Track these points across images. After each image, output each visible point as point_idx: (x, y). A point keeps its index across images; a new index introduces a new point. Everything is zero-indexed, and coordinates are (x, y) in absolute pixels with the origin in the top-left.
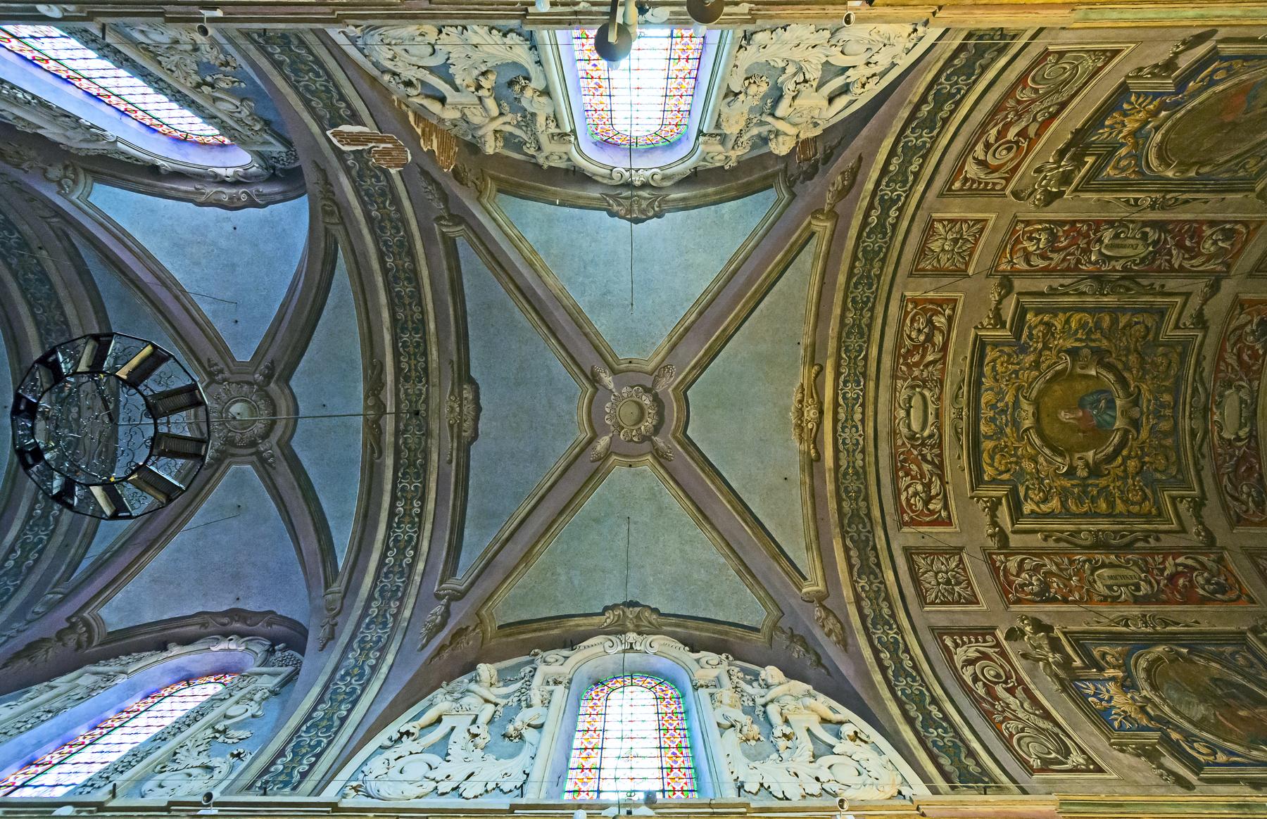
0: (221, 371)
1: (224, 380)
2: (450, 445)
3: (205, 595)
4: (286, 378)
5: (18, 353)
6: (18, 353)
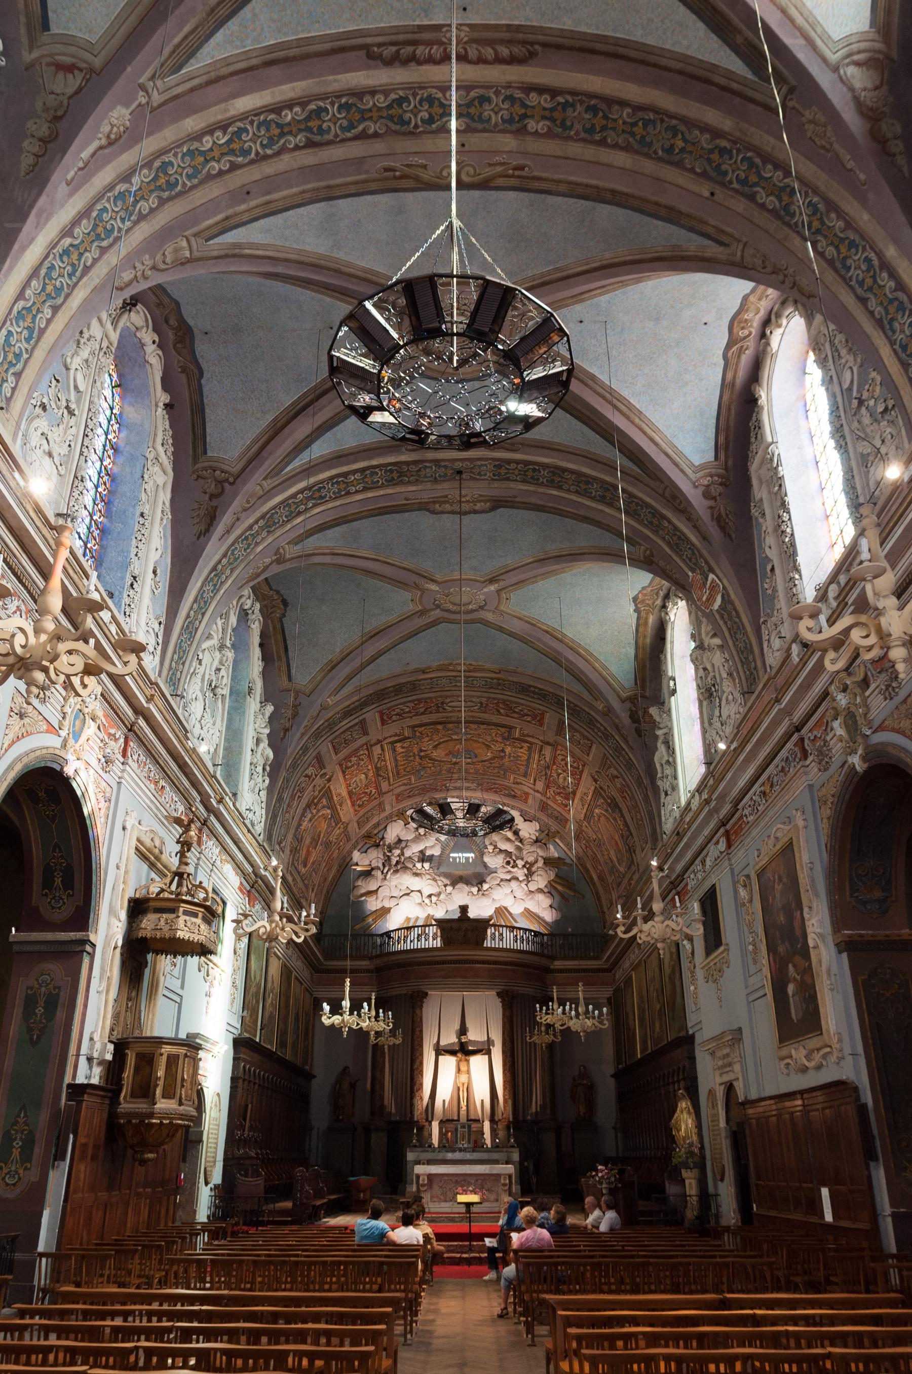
2: (426, 497)
5: (559, 47)
6: (559, 47)
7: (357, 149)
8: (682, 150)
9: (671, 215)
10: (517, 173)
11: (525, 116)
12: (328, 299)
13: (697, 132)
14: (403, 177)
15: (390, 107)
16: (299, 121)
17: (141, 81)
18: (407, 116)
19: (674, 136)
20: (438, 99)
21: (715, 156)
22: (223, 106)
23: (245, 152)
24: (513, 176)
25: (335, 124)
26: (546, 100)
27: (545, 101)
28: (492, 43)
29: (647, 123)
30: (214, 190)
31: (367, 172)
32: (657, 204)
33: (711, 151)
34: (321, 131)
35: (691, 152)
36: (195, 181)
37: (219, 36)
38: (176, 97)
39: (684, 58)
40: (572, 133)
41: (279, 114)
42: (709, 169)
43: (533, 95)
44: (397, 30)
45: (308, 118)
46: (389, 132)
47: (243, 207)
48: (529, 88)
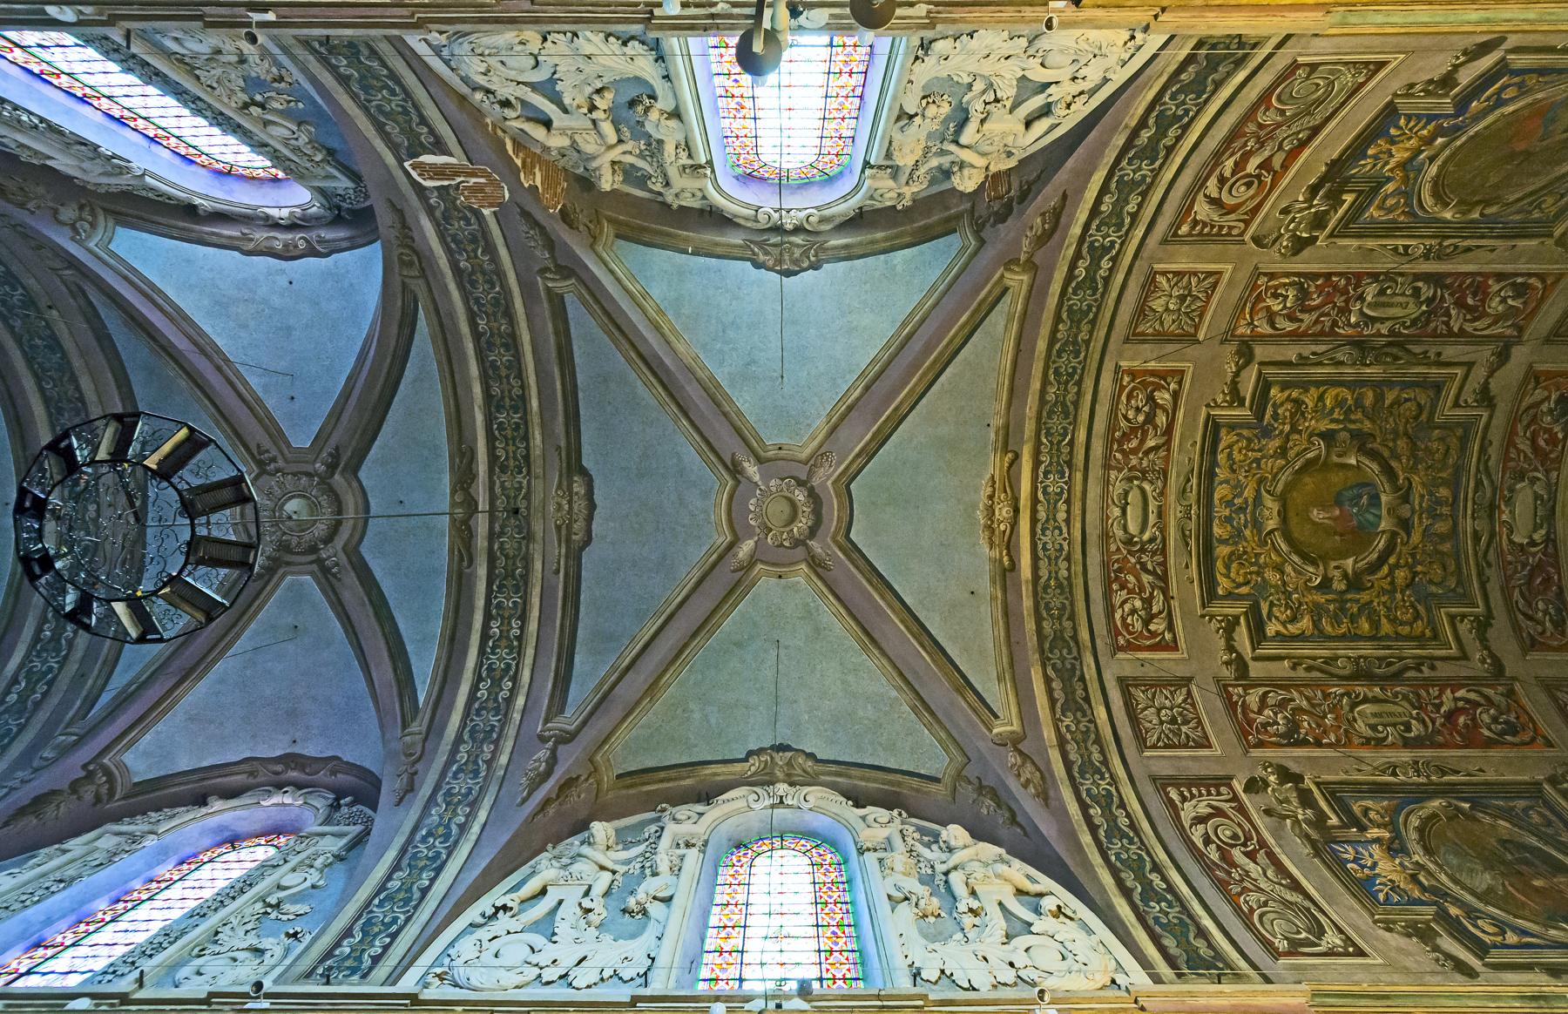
0: (274, 460)
1: (278, 471)
3: (254, 737)
4: (354, 468)
5: (22, 437)
6: (22, 437)
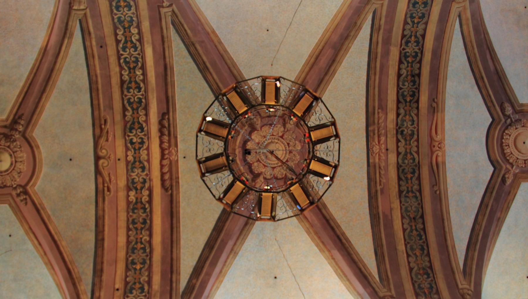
0: (18, 195)
1: (15, 188)
5: (171, 202)
6: (171, 202)
7: (117, 105)
8: (135, 269)
9: (98, 272)
10: (106, 189)
11: (136, 189)
12: (21, 84)
13: (147, 274)
14: (101, 129)
15: (139, 123)
16: (135, 78)
17: (174, 6)
18: (134, 132)
19: (141, 264)
20: (143, 147)
21: (138, 286)
22: (150, 41)
23: (124, 49)
24: (104, 186)
25: (132, 95)
26: (146, 199)
27: (145, 199)
28: (170, 171)
29: (144, 249)
30: (108, 29)
31: (105, 110)
32: (102, 263)
33: (140, 283)
34: (129, 88)
35: (135, 273)
36: (116, 21)
37: (182, 45)
38: (160, 19)
39: (178, 259)
40: (131, 214)
41: (140, 68)
42: (130, 284)
43: (147, 192)
44: (175, 127)
45: (136, 83)
46: (126, 123)
47: (94, 43)
48: (150, 190)
